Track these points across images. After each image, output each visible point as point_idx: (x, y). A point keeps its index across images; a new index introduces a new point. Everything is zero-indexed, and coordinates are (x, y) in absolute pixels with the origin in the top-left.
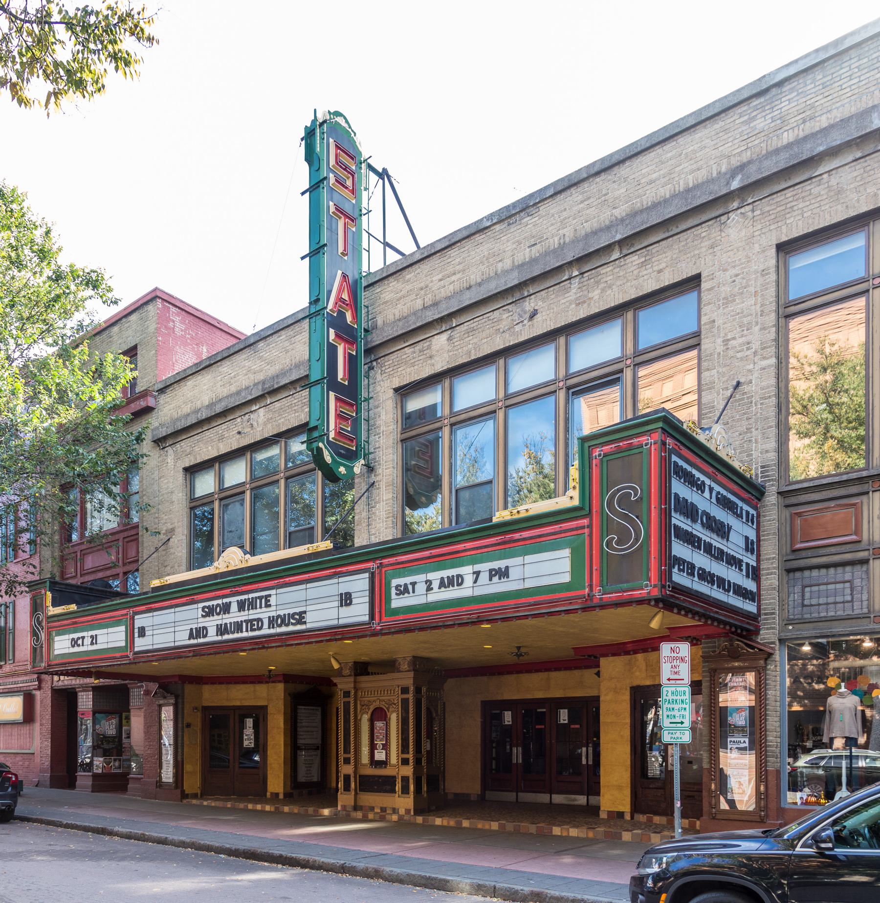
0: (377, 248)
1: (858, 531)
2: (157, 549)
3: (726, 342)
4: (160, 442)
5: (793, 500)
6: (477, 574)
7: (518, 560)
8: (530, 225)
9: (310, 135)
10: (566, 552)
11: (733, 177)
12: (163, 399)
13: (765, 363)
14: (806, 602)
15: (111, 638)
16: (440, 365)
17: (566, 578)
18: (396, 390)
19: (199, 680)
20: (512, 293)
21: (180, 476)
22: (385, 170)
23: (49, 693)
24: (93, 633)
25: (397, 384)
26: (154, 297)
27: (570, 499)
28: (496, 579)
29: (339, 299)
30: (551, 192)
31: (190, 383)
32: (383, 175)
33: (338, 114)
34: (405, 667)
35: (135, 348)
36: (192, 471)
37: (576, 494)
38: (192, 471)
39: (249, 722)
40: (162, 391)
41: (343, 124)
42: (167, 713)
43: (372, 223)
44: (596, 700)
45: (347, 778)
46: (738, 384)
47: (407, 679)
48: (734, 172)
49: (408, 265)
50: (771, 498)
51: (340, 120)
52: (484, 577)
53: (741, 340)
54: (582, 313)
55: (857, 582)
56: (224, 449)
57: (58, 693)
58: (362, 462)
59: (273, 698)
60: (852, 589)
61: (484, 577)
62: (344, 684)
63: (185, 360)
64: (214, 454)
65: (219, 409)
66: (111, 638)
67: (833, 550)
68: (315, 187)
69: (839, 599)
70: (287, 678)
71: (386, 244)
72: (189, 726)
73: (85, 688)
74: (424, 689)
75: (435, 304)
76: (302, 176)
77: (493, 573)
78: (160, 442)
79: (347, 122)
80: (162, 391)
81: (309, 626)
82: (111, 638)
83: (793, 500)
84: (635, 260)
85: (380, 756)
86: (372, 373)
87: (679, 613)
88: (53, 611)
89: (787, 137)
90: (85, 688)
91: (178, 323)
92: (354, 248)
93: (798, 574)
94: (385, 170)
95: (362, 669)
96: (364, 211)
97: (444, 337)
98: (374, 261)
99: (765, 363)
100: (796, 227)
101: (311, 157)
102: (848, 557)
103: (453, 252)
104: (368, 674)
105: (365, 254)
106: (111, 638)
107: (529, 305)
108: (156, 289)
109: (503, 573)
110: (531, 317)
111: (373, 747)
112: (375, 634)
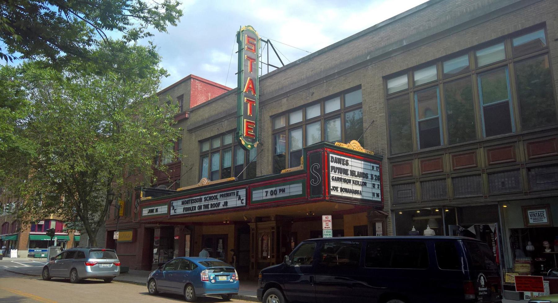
0: (265, 67)
1: (412, 172)
2: (187, 172)
3: (369, 107)
4: (190, 131)
5: (393, 161)
6: (267, 192)
7: (288, 186)
8: (312, 64)
9: (238, 35)
10: (301, 185)
11: (368, 55)
12: (192, 115)
13: (381, 115)
14: (399, 196)
15: (163, 210)
16: (284, 109)
17: (301, 193)
18: (271, 117)
19: (200, 224)
20: (308, 86)
21: (197, 144)
22: (268, 40)
23: (143, 230)
24: (156, 208)
25: (271, 114)
26: (189, 78)
27: (300, 168)
28: (281, 192)
29: (248, 87)
30: (317, 54)
31: (202, 110)
32: (268, 42)
33: (249, 26)
34: (273, 219)
35: (183, 95)
36: (201, 142)
37: (302, 165)
38: (201, 142)
39: (221, 241)
40: (192, 112)
41: (252, 29)
42: (188, 237)
43: (264, 59)
44: (343, 230)
45: (253, 263)
46: (373, 121)
47: (273, 224)
48: (369, 53)
49: (279, 71)
50: (385, 160)
51: (249, 28)
52: (269, 194)
53: (373, 107)
54: (327, 95)
55: (413, 190)
56: (212, 135)
57: (147, 229)
58: (258, 142)
59: (230, 231)
60: (412, 192)
61: (269, 194)
62: (252, 225)
63: (201, 100)
64: (209, 136)
65: (211, 120)
66: (163, 210)
67: (404, 178)
68: (240, 51)
69: (408, 196)
70: (235, 223)
71: (268, 65)
72: (196, 243)
73: (158, 228)
74: (281, 228)
75: (282, 88)
76: (236, 47)
77: (280, 190)
78: (190, 131)
79: (252, 28)
80: (192, 112)
81: (228, 207)
82: (163, 210)
83: (393, 161)
84: (342, 78)
85: (265, 254)
86: (262, 110)
87: (226, 221)
88: (143, 198)
89: (383, 44)
90: (158, 228)
91: (199, 85)
92: (254, 69)
93: (396, 187)
94: (268, 40)
95: (259, 219)
96: (260, 55)
97: (285, 99)
98: (263, 71)
99: (381, 115)
100: (388, 72)
101: (239, 41)
102: (410, 181)
103: (288, 71)
104: (261, 221)
105: (260, 70)
106: (163, 210)
107: (311, 91)
108: (190, 75)
109: (283, 191)
110: (312, 95)
111: (262, 251)
112: (248, 210)
